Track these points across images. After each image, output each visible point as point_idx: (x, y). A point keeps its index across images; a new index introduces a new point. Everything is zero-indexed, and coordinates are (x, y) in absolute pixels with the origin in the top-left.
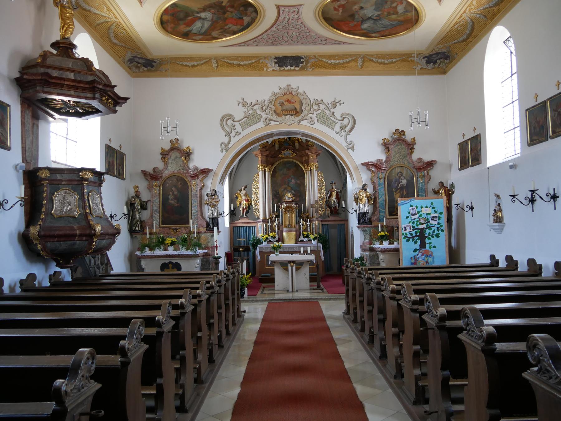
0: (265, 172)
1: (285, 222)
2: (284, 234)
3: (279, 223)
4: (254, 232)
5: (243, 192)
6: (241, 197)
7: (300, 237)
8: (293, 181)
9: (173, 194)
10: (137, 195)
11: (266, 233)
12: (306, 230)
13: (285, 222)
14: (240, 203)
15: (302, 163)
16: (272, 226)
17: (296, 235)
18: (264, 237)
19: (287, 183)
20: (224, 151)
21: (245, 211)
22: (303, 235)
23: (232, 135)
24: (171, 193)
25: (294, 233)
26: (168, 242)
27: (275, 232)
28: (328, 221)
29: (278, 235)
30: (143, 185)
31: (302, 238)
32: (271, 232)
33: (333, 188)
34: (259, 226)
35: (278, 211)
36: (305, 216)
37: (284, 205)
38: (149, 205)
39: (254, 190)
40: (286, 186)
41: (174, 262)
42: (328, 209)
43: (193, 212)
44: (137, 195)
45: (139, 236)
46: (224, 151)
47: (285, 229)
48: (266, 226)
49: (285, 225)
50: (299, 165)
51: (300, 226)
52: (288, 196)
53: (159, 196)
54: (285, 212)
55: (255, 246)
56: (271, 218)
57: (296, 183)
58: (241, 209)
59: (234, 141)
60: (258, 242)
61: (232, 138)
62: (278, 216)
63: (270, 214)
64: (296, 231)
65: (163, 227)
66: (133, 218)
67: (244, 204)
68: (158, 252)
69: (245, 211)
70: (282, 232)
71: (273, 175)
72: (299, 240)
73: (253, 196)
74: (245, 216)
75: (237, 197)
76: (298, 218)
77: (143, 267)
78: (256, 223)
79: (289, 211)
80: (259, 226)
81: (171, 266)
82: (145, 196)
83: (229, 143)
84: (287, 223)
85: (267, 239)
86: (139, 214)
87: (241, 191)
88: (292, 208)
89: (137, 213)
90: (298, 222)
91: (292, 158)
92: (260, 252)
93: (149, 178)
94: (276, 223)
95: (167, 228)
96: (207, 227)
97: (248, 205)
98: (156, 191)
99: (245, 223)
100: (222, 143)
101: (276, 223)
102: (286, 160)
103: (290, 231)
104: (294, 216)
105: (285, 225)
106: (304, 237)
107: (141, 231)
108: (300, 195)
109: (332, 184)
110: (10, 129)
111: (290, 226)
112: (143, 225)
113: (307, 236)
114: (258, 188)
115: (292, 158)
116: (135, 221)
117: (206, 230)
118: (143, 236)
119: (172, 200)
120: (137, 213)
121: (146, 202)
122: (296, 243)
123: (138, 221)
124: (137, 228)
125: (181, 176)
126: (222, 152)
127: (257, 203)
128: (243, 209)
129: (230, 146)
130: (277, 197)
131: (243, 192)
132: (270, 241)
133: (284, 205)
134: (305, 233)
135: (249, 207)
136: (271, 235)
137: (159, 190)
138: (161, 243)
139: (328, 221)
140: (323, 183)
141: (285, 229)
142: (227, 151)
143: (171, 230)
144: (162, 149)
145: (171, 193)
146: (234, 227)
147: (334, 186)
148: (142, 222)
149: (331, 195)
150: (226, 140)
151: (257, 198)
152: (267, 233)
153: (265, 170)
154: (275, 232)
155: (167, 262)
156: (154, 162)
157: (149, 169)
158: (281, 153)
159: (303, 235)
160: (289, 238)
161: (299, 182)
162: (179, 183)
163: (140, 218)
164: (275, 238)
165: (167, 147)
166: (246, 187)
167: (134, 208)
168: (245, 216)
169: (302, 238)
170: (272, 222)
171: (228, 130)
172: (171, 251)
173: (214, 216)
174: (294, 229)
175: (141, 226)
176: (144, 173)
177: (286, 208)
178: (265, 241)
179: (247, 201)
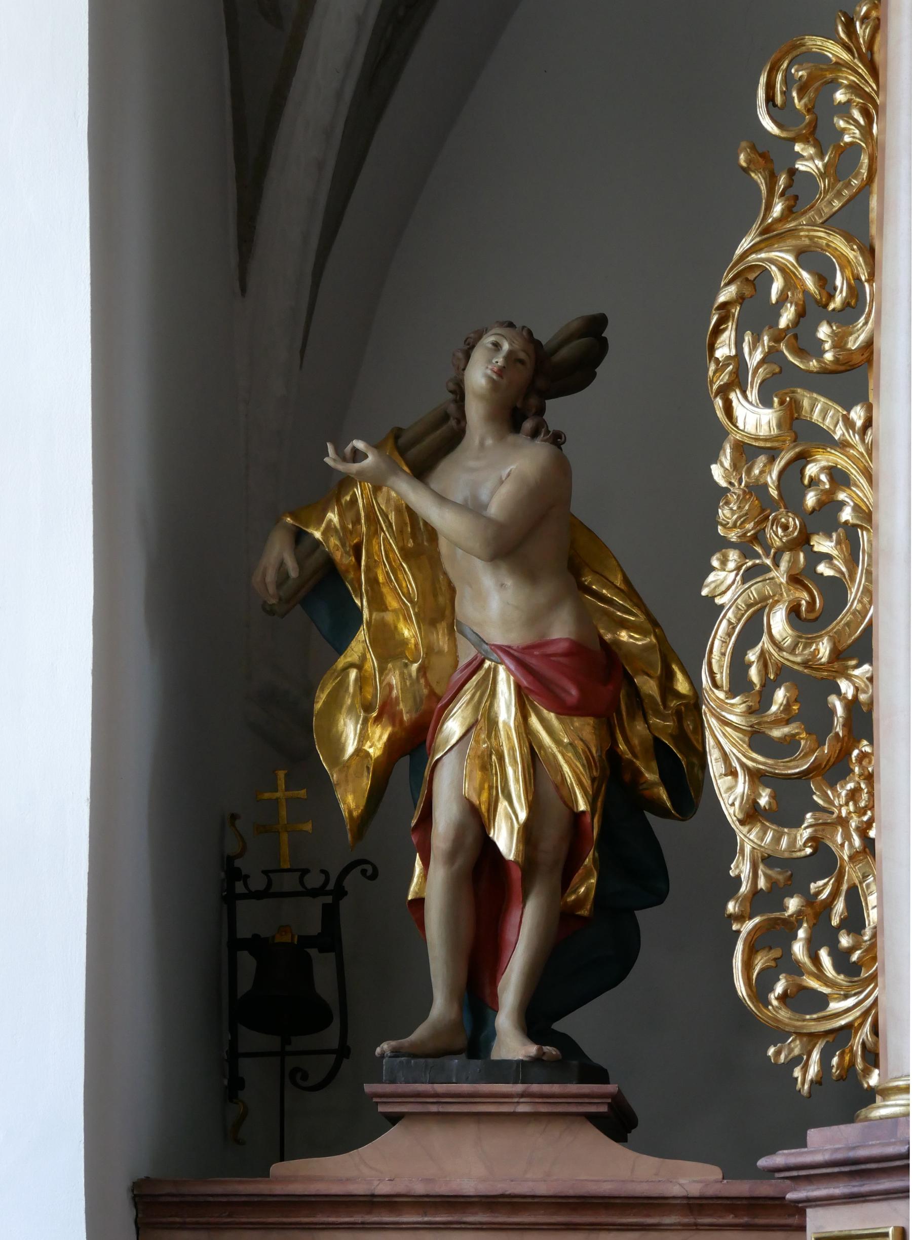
5: (494, 473)
6: (439, 606)
14: (413, 746)
58: (431, 883)
67: (499, 763)
73: (723, 580)
74: (511, 1043)
75: (327, 598)
87: (428, 448)
97: (612, 775)
128: (486, 880)
131: (494, 473)
168: (511, 1043)
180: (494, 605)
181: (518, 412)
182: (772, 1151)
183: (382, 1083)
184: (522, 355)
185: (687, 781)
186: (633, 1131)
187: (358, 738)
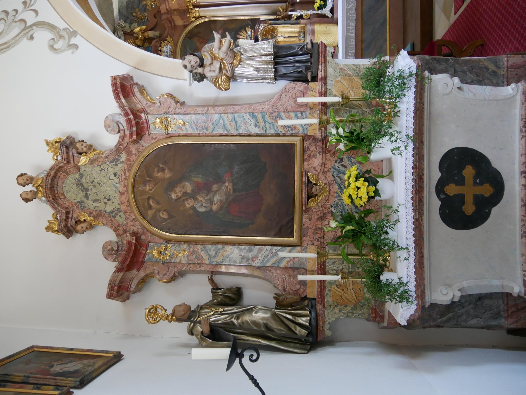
7: (324, 16)
9: (193, 196)
10: (187, 315)
15: (185, 26)
17: (320, 23)
20: (73, 41)
23: (30, 18)
24: (189, 204)
26: (363, 192)
30: (164, 295)
31: (326, 11)
38: (225, 282)
41: (437, 175)
43: (254, 130)
44: (187, 315)
45: (330, 316)
46: (73, 41)
50: (190, 32)
53: (197, 242)
59: (48, 14)
61: (40, 19)
64: (313, 23)
65: (302, 236)
66: (264, 332)
68: (402, 232)
72: (330, 15)
77: (458, 294)
81: (452, 189)
82: (196, 291)
83: (51, 27)
86: (250, 311)
89: (247, 318)
93: (136, 275)
95: (305, 220)
96: (306, 81)
98: (181, 254)
100: (52, 47)
106: (325, 6)
107: (314, 307)
112: (291, 298)
115: (175, 45)
116: (274, 325)
117: (314, 79)
118: (329, 299)
119: (211, 202)
120: (247, 318)
121: (216, 288)
122: (336, 23)
123: (275, 316)
124: (303, 321)
125: (135, 168)
126: (76, 46)
129: (61, 25)
137: (179, 242)
138: (364, 229)
142: (74, 34)
143: (312, 204)
144: (48, 229)
145: (189, 204)
148: (280, 304)
150: (43, 36)
155: (437, 203)
156: (91, 256)
157: (109, 267)
162: (159, 175)
163: (266, 309)
165: (42, 211)
167: (228, 326)
169: (326, 11)
171: (16, 30)
172: (398, 190)
173: (271, 50)
175: (292, 305)
176: (119, 290)
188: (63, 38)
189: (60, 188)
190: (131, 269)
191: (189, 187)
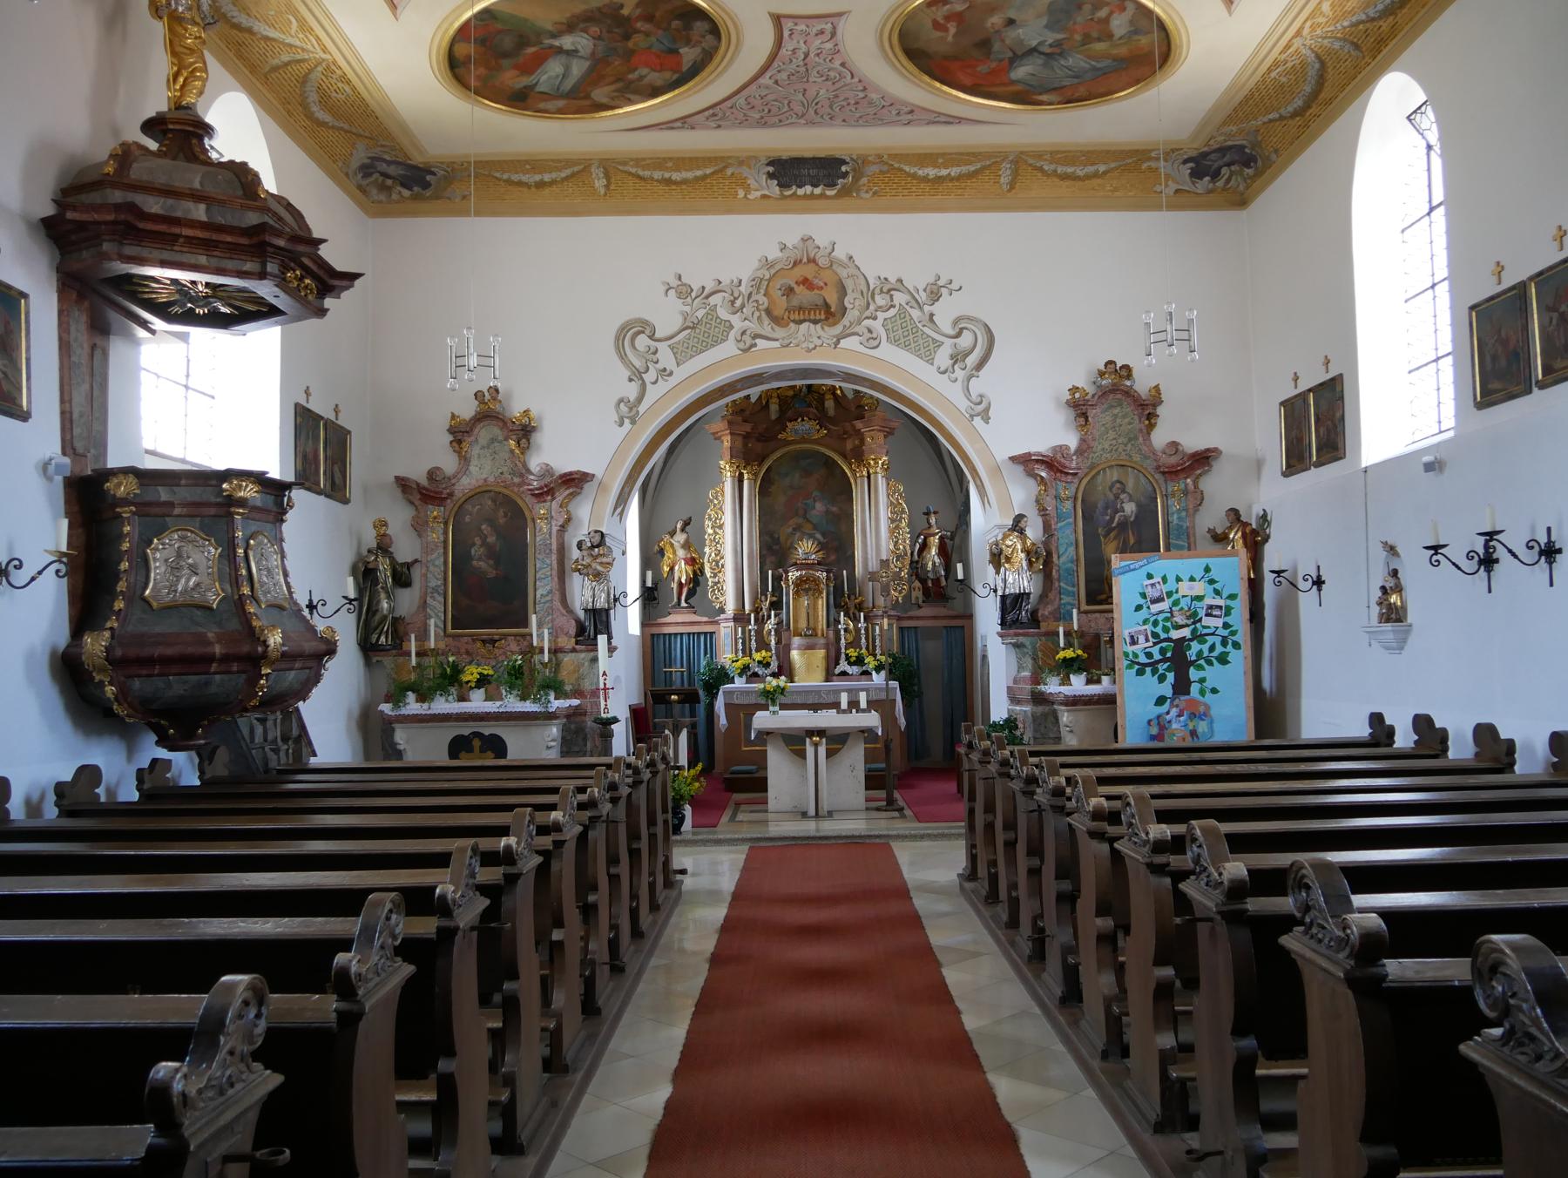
0: (741, 481)
1: (796, 621)
2: (795, 654)
3: (779, 623)
4: (711, 649)
5: (680, 538)
6: (674, 553)
7: (837, 663)
8: (819, 506)
9: (484, 543)
10: (383, 547)
11: (744, 651)
12: (854, 644)
13: (796, 621)
14: (672, 569)
15: (844, 456)
16: (759, 633)
17: (827, 657)
18: (739, 664)
19: (801, 512)
20: (627, 421)
21: (685, 591)
22: (848, 657)
23: (649, 377)
24: (478, 541)
25: (821, 653)
27: (768, 649)
28: (918, 618)
29: (778, 658)
30: (399, 518)
31: (843, 666)
32: (758, 650)
33: (930, 526)
34: (725, 631)
35: (777, 589)
36: (851, 605)
37: (793, 575)
38: (416, 574)
39: (710, 531)
40: (800, 520)
41: (487, 732)
42: (917, 584)
43: (539, 593)
44: (383, 547)
45: (388, 661)
46: (627, 421)
47: (796, 641)
48: (743, 632)
49: (796, 628)
50: (835, 462)
51: (837, 632)
52: (805, 548)
53: (445, 548)
54: (797, 593)
55: (712, 688)
56: (757, 610)
57: (827, 512)
58: (675, 586)
59: (653, 394)
60: (722, 676)
61: (649, 386)
62: (776, 605)
63: (754, 600)
64: (827, 646)
65: (454, 636)
66: (372, 610)
67: (682, 572)
68: (443, 705)
69: (685, 591)
70: (788, 648)
71: (764, 490)
72: (837, 671)
73: (707, 550)
74: (683, 604)
75: (662, 552)
76: (833, 610)
77: (401, 748)
78: (717, 623)
79: (806, 591)
80: (725, 631)
81: (477, 743)
82: (405, 549)
83: (640, 399)
84: (803, 624)
85: (746, 668)
86: (389, 597)
87: (672, 534)
88: (816, 581)
89: (383, 595)
90: (833, 623)
91: (816, 442)
92: (726, 705)
93: (416, 497)
94: (770, 625)
95: (465, 639)
96: (577, 635)
97: (695, 572)
98: (435, 536)
99: (684, 624)
100: (621, 400)
101: (770, 625)
102: (798, 446)
103: (810, 647)
104: (821, 604)
105: (796, 628)
106: (850, 664)
107: (394, 648)
108: (838, 546)
109: (927, 514)
110: (28, 360)
111: (811, 633)
112: (401, 629)
113: (859, 661)
114: (721, 527)
115: (816, 442)
116: (377, 617)
117: (577, 643)
118: (401, 659)
119: (480, 559)
120: (383, 595)
121: (409, 566)
122: (827, 680)
123: (385, 617)
124: (383, 639)
125: (506, 492)
126: (621, 424)
127: (718, 567)
128: (681, 585)
129: (642, 408)
130: (773, 552)
131: (680, 538)
132: (755, 675)
133: (793, 575)
134: (853, 653)
135: (696, 580)
136: (757, 656)
137: (446, 533)
138: (450, 680)
139: (918, 618)
140: (903, 512)
141: (796, 641)
142: (633, 422)
143: (479, 644)
144: (453, 417)
145: (478, 541)
146: (653, 635)
147: (933, 520)
148: (396, 621)
149: (924, 546)
150: (632, 391)
151: (718, 553)
152: (747, 652)
153: (741, 477)
154: (768, 649)
155: (466, 732)
156: (431, 453)
157: (418, 473)
158: (784, 429)
159: (848, 657)
160: (809, 667)
161: (834, 509)
162: (501, 513)
163: (392, 610)
164: (767, 665)
165: (468, 410)
166: (687, 523)
167: (376, 582)
168: (683, 604)
169: (843, 666)
170: (761, 622)
171: (638, 363)
172: (478, 703)
174: (822, 641)
175: (395, 632)
176: (403, 484)
177: (799, 583)
178: (740, 675)
179: (691, 561)
180: (681, 553)
181: (683, 530)
182: (896, 719)
183: (1531, 279)
184: (679, 877)
185: (702, 572)
186: (238, 160)
187: (666, 569)
188: (629, 411)
189: (495, 422)
190: (425, 494)
191: (491, 539)
